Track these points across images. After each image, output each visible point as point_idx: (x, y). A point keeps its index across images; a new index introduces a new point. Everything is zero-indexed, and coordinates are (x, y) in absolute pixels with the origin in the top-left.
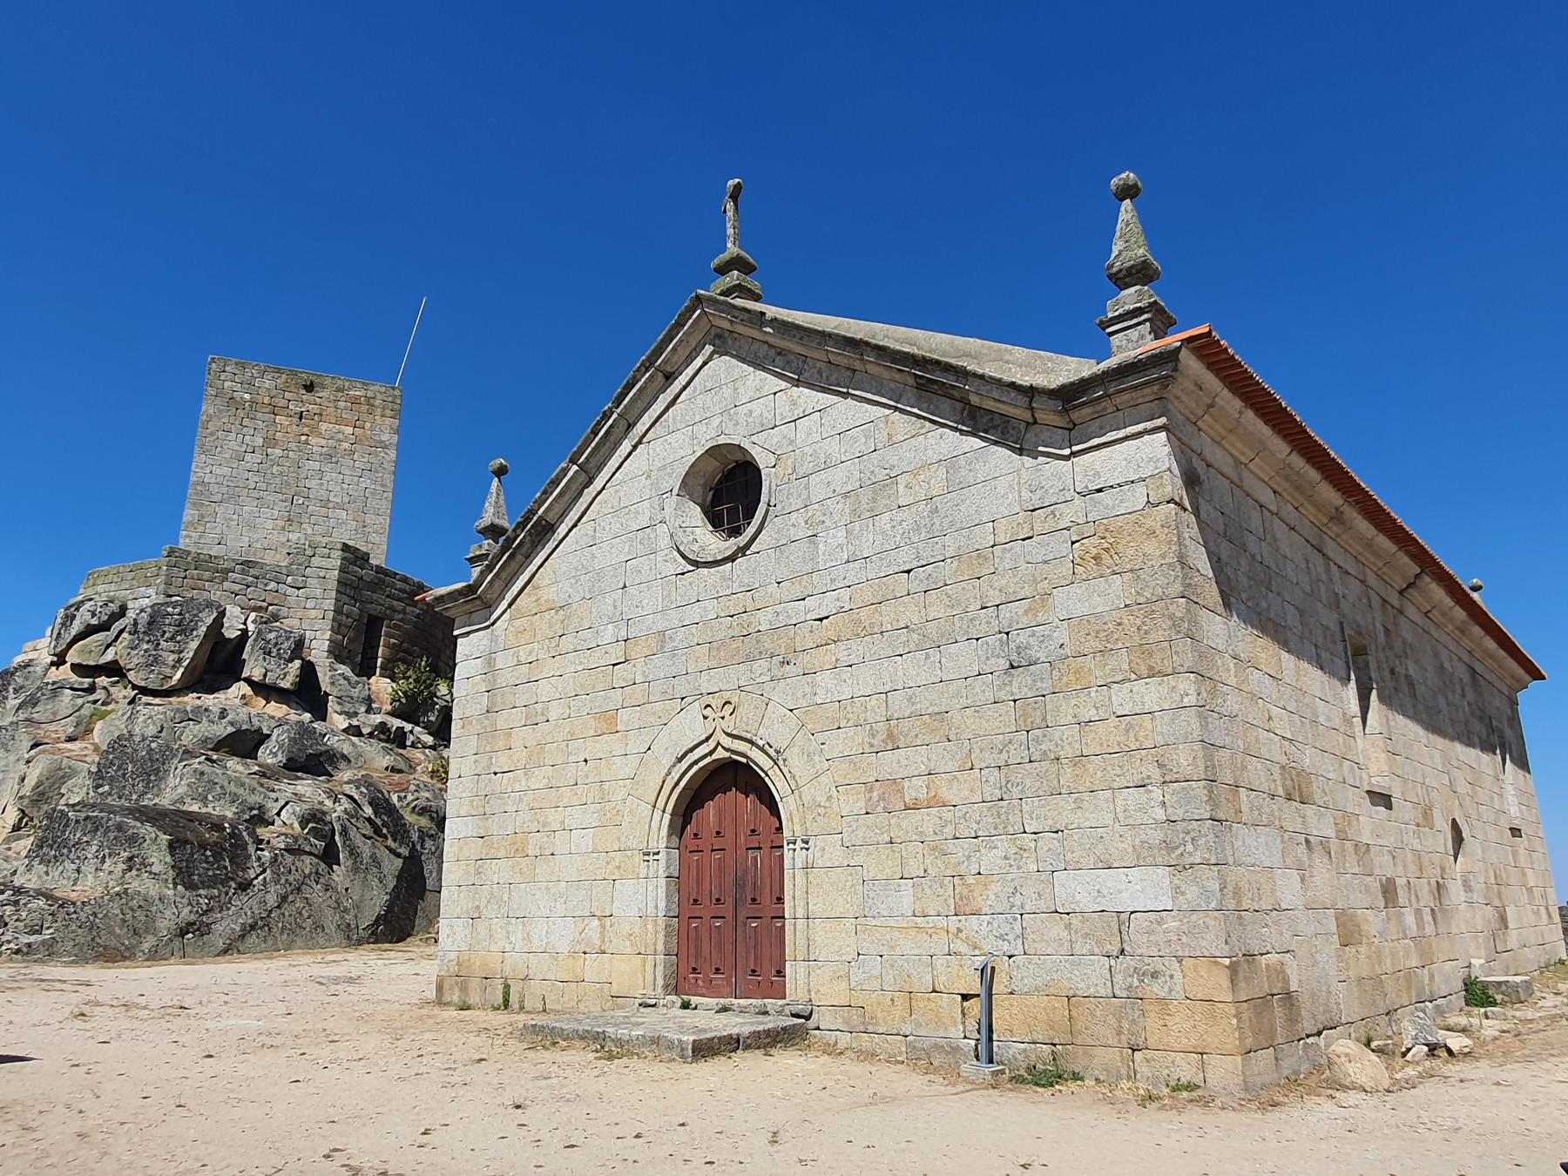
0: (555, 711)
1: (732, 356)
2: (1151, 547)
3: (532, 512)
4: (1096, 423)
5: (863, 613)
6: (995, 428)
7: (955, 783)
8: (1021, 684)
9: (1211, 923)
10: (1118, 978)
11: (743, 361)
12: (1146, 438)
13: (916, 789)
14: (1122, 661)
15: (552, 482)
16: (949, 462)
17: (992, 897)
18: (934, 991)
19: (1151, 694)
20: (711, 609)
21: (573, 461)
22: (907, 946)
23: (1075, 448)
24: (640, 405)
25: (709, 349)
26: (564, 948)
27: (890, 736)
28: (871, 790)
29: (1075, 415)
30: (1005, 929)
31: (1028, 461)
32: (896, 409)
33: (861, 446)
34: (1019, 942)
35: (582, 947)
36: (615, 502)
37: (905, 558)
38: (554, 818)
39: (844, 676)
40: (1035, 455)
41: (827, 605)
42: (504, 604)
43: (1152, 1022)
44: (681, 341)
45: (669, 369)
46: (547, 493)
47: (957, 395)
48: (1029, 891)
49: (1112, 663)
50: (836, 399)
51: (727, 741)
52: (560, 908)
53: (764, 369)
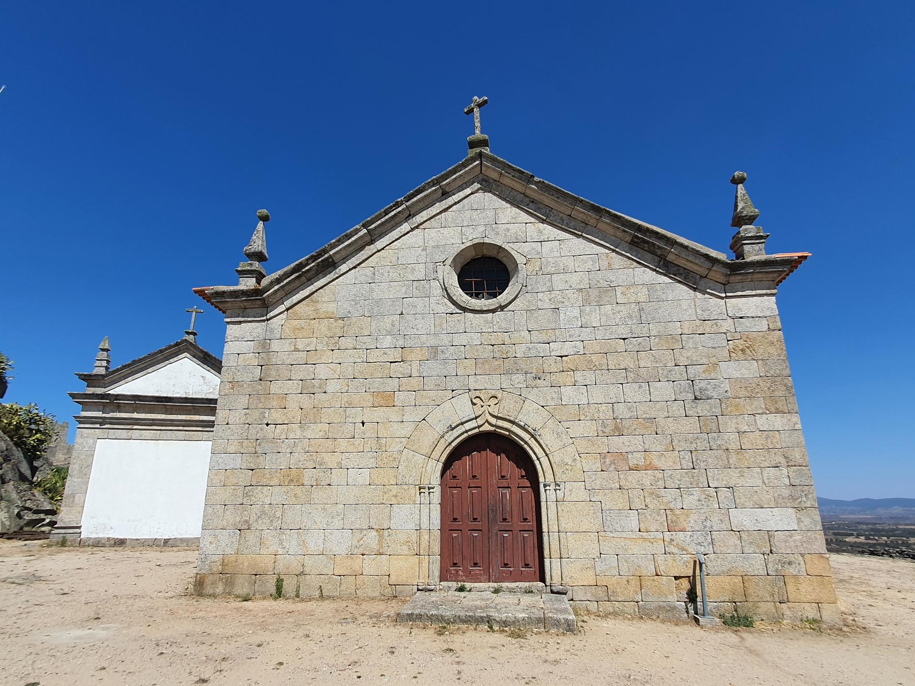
0: (332, 387)
1: (495, 194)
2: (772, 350)
3: (325, 251)
4: (740, 285)
5: (594, 357)
6: (681, 274)
7: (663, 458)
8: (702, 408)
9: (818, 537)
10: (770, 565)
11: (504, 199)
12: (765, 297)
13: (636, 459)
14: (760, 404)
15: (346, 236)
16: (650, 287)
17: (693, 521)
18: (657, 575)
19: (777, 421)
20: (476, 339)
21: (364, 226)
22: (635, 549)
23: (728, 294)
24: (421, 205)
25: (477, 186)
26: (342, 550)
27: (617, 428)
28: (605, 458)
29: (732, 279)
30: (701, 539)
31: (699, 295)
32: (613, 251)
33: (589, 265)
34: (711, 546)
35: (361, 551)
36: (394, 259)
37: (623, 331)
38: (331, 460)
39: (581, 391)
40: (704, 292)
41: (567, 349)
42: (282, 308)
43: (791, 588)
44: (461, 175)
45: (447, 189)
46: (340, 242)
47: (659, 252)
48: (715, 519)
49: (756, 403)
50: (571, 236)
51: (493, 421)
52: (337, 523)
53: (518, 207)
